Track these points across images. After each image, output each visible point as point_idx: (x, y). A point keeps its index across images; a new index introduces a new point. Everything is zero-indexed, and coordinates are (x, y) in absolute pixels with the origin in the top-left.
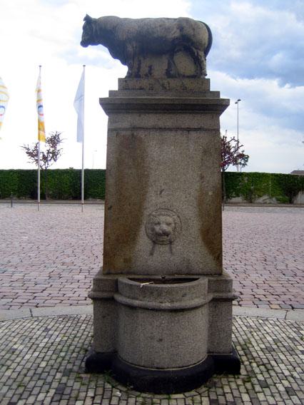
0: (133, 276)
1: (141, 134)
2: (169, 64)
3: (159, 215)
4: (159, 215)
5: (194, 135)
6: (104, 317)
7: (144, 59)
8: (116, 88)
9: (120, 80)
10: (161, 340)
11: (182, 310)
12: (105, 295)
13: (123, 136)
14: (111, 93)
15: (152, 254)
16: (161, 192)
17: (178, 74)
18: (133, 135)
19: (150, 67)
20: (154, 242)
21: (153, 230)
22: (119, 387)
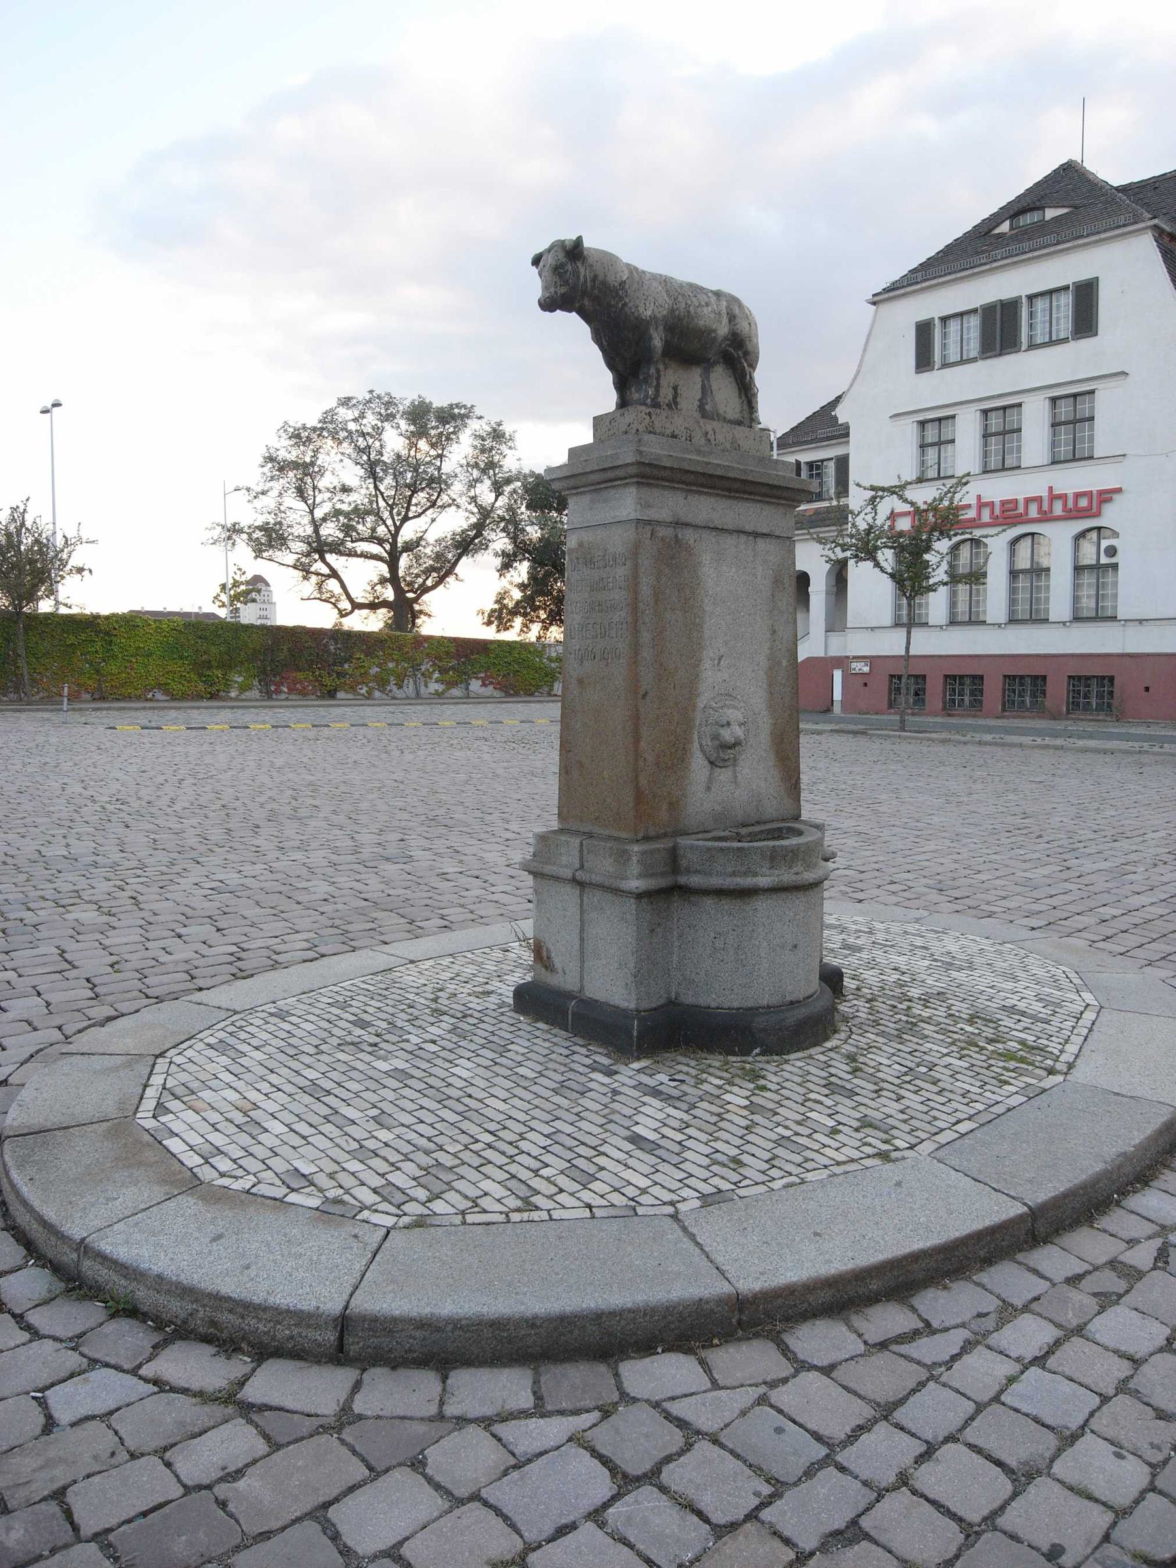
0: (709, 835)
1: (689, 535)
2: (703, 388)
3: (722, 708)
4: (722, 708)
5: (762, 544)
6: (652, 931)
7: (666, 368)
8: (585, 436)
9: (598, 421)
10: (795, 946)
11: (745, 894)
12: (663, 882)
13: (662, 539)
14: (573, 452)
15: (708, 789)
16: (720, 660)
17: (718, 415)
18: (676, 536)
19: (675, 388)
20: (711, 763)
21: (716, 737)
22: (793, 1056)
